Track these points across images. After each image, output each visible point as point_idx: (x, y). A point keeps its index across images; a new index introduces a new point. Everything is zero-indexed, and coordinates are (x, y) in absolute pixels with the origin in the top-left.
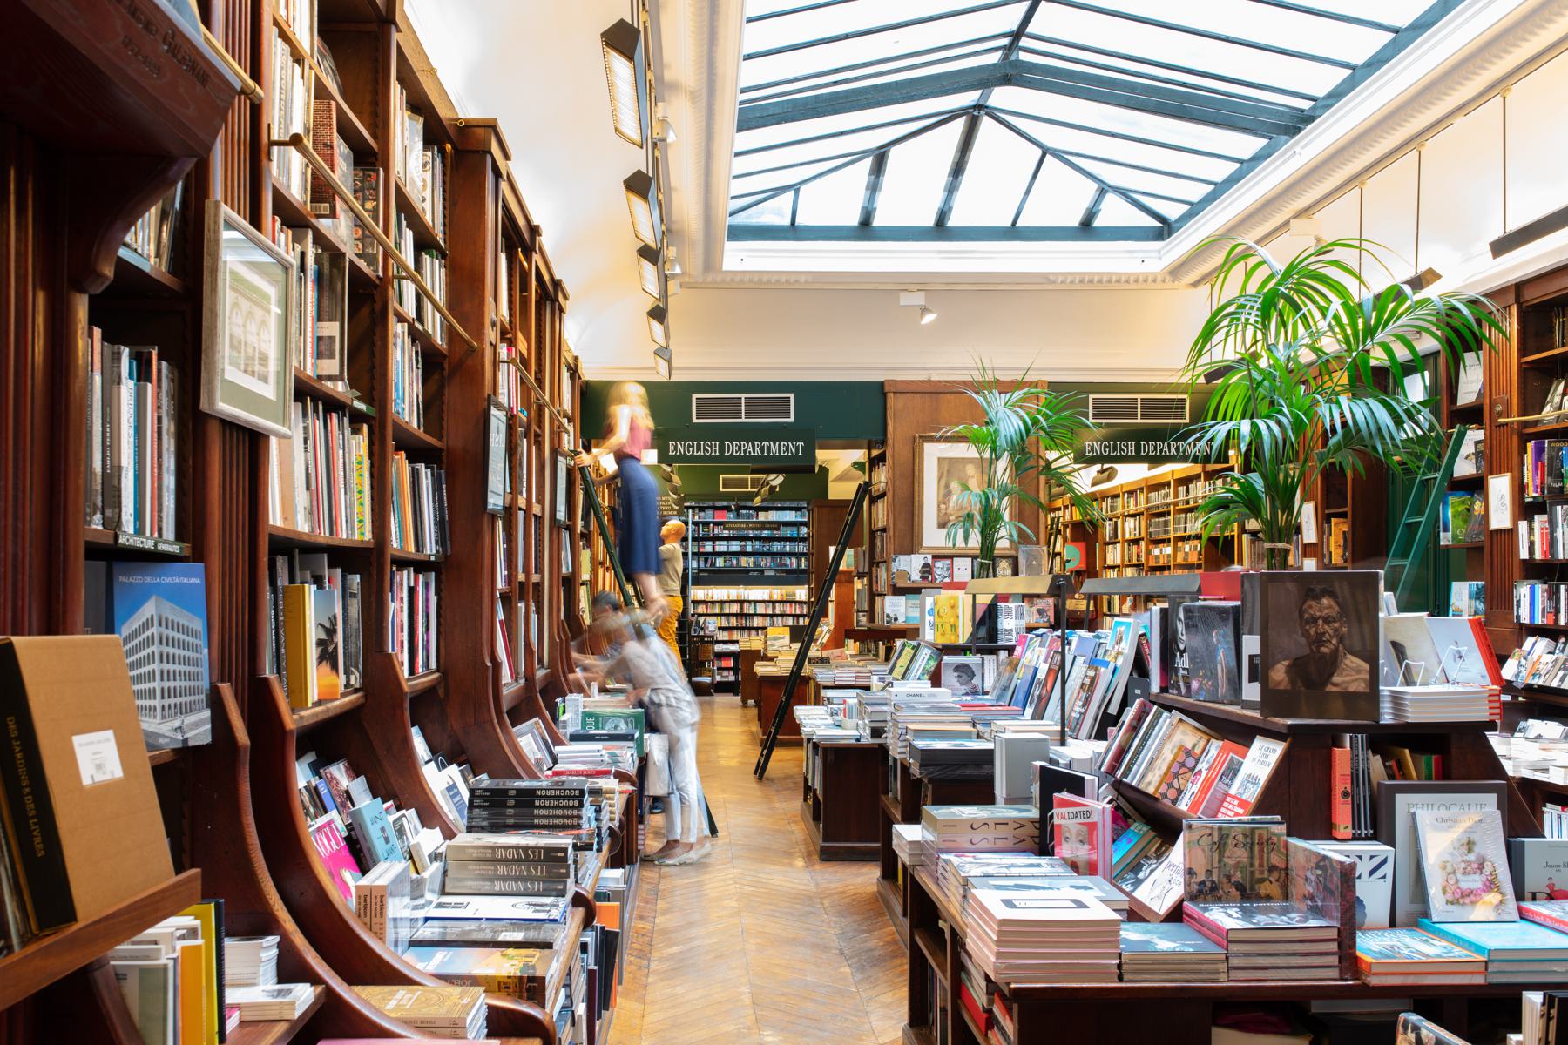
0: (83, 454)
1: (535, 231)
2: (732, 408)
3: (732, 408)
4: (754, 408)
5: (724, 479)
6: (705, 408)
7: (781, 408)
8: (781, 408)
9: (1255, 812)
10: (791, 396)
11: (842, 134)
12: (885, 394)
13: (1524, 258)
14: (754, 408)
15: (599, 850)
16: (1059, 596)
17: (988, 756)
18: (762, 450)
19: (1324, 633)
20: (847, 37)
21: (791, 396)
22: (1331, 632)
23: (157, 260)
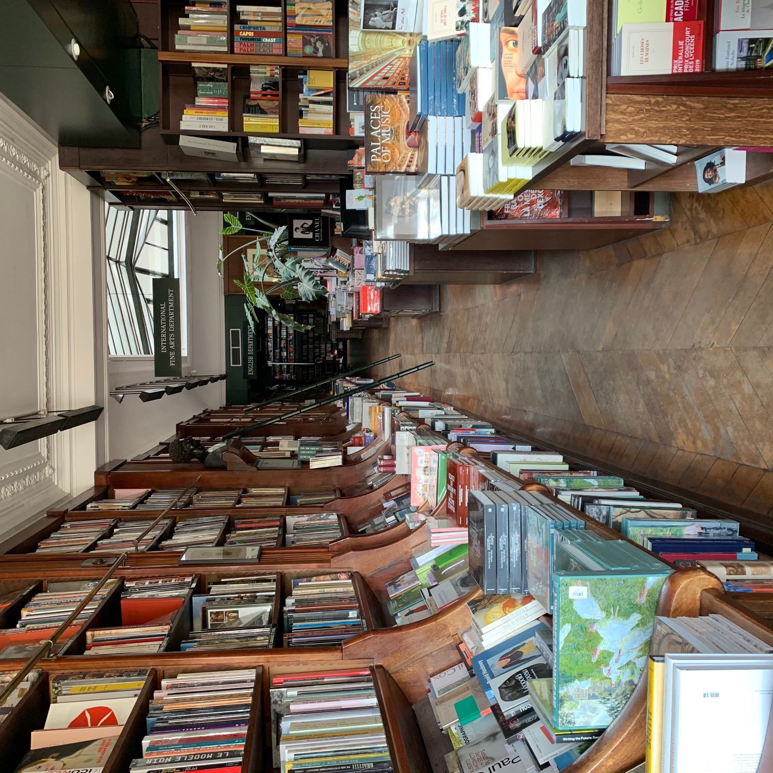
0: (132, 720)
1: (194, 417)
2: (236, 352)
3: (236, 352)
4: (236, 343)
5: (233, 364)
6: (236, 361)
7: (235, 334)
8: (235, 334)
9: (558, 547)
10: (231, 330)
11: (123, 320)
12: (229, 295)
13: (218, 47)
14: (236, 343)
15: (237, 612)
16: (603, 350)
17: (371, 239)
18: (251, 341)
19: (410, 204)
20: (123, 320)
21: (231, 330)
22: (409, 201)
23: (288, 455)
